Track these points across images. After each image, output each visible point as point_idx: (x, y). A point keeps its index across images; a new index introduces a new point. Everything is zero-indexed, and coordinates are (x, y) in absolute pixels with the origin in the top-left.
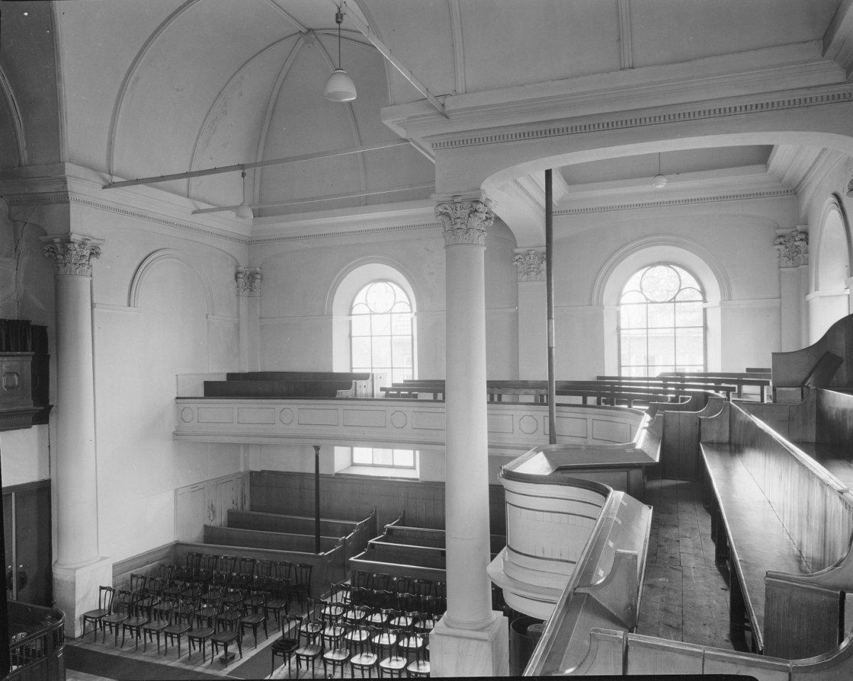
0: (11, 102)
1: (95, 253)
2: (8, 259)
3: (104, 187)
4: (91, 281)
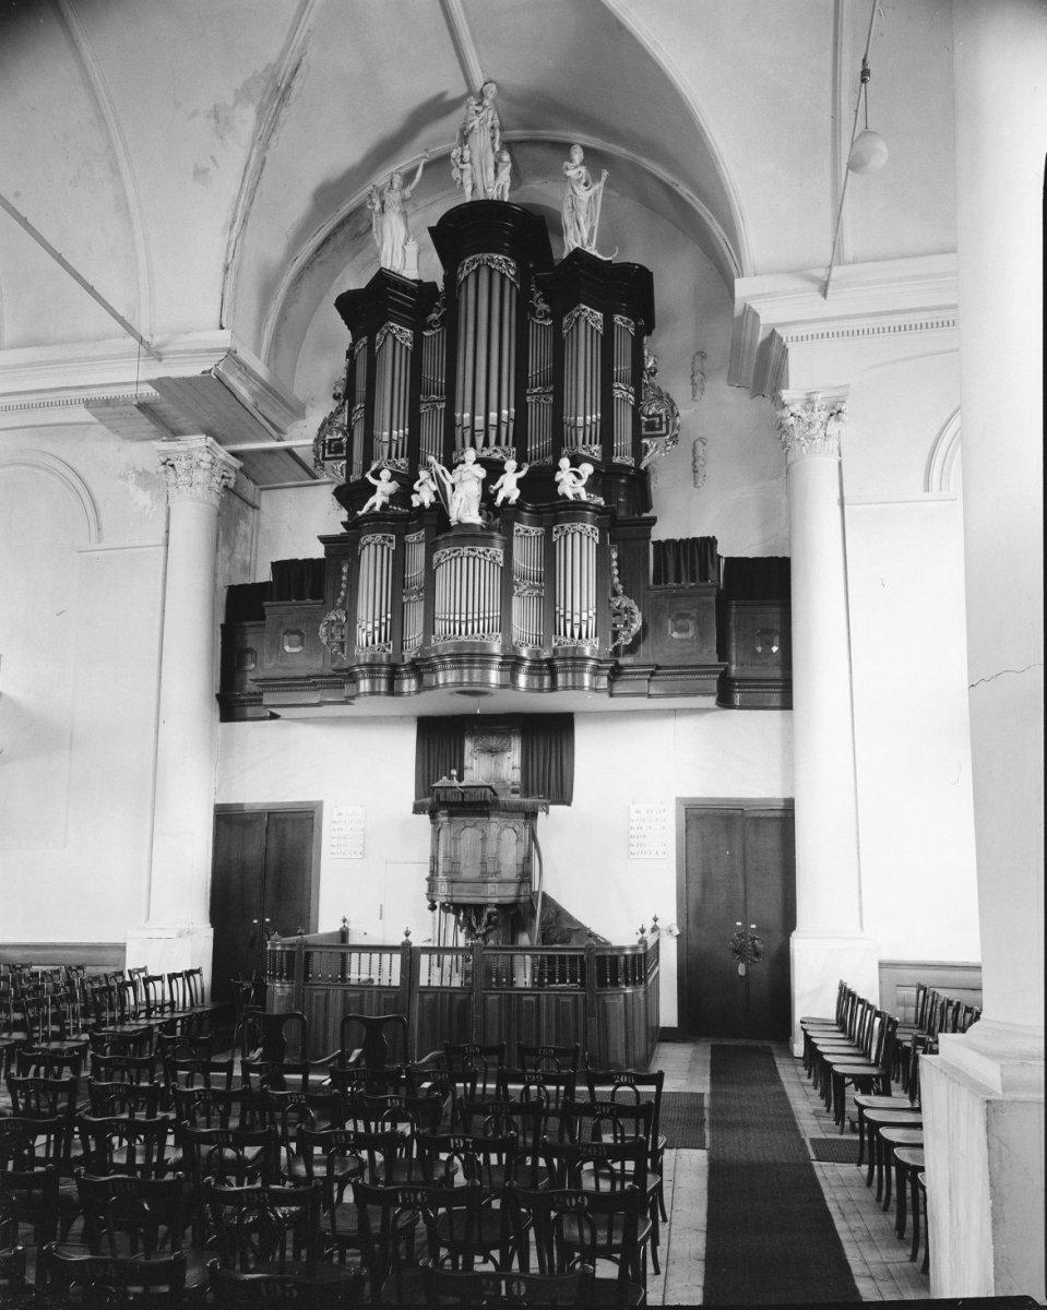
1: (835, 413)
2: (774, 481)
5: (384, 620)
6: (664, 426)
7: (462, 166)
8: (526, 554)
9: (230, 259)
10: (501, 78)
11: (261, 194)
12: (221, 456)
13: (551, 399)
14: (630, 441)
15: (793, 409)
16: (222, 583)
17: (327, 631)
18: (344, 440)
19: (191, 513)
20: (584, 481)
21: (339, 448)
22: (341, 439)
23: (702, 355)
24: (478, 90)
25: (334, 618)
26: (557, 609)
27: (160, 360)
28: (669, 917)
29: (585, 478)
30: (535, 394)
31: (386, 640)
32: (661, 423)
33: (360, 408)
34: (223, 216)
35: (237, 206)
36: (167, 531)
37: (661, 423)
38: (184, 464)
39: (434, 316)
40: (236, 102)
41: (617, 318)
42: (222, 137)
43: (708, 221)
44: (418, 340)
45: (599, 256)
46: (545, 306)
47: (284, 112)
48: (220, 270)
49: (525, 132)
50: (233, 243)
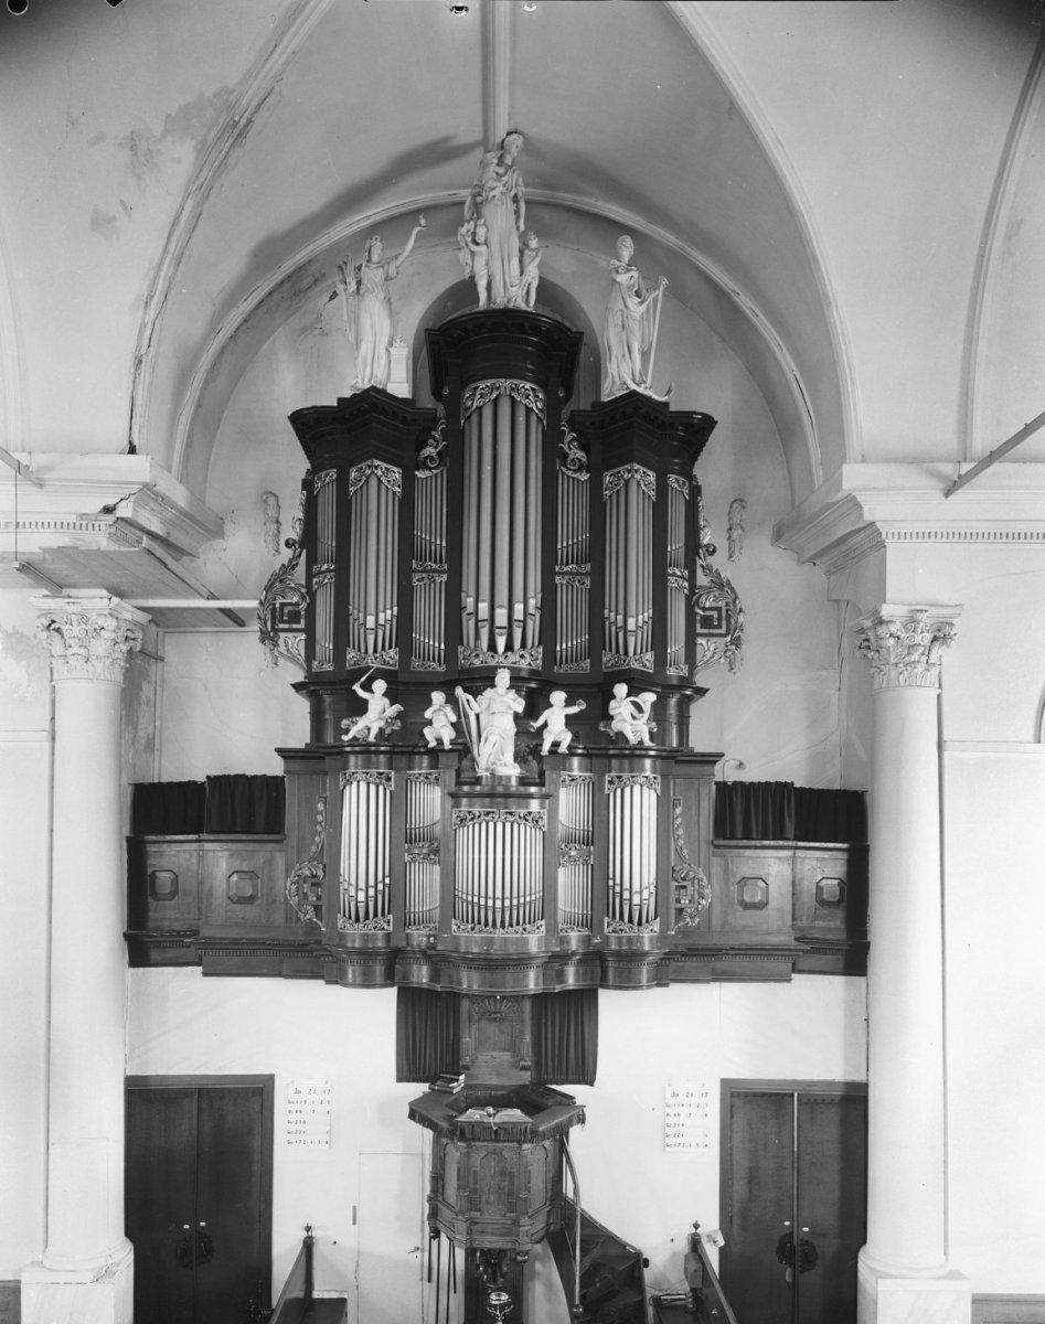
0: (795, 386)
1: (940, 636)
2: (824, 673)
3: (948, 493)
4: (939, 696)
5: (380, 887)
6: (724, 623)
7: (473, 248)
8: (570, 805)
9: (143, 351)
10: (531, 131)
11: (190, 257)
12: (128, 616)
13: (588, 582)
14: (683, 644)
15: (893, 628)
16: (125, 781)
17: (298, 889)
18: (303, 606)
19: (87, 701)
20: (646, 715)
21: (294, 617)
22: (297, 604)
23: (739, 501)
24: (499, 140)
25: (308, 873)
26: (611, 883)
27: (41, 486)
28: (711, 1223)
29: (647, 708)
30: (567, 573)
31: (383, 914)
32: (720, 619)
33: (328, 571)
34: (136, 286)
35: (156, 276)
36: (53, 719)
37: (720, 619)
38: (76, 630)
39: (429, 451)
40: (166, 132)
41: (672, 477)
42: (140, 178)
43: (777, 350)
44: (409, 482)
45: (655, 397)
46: (580, 454)
47: (237, 152)
48: (127, 363)
49: (538, 191)
50: (149, 326)
